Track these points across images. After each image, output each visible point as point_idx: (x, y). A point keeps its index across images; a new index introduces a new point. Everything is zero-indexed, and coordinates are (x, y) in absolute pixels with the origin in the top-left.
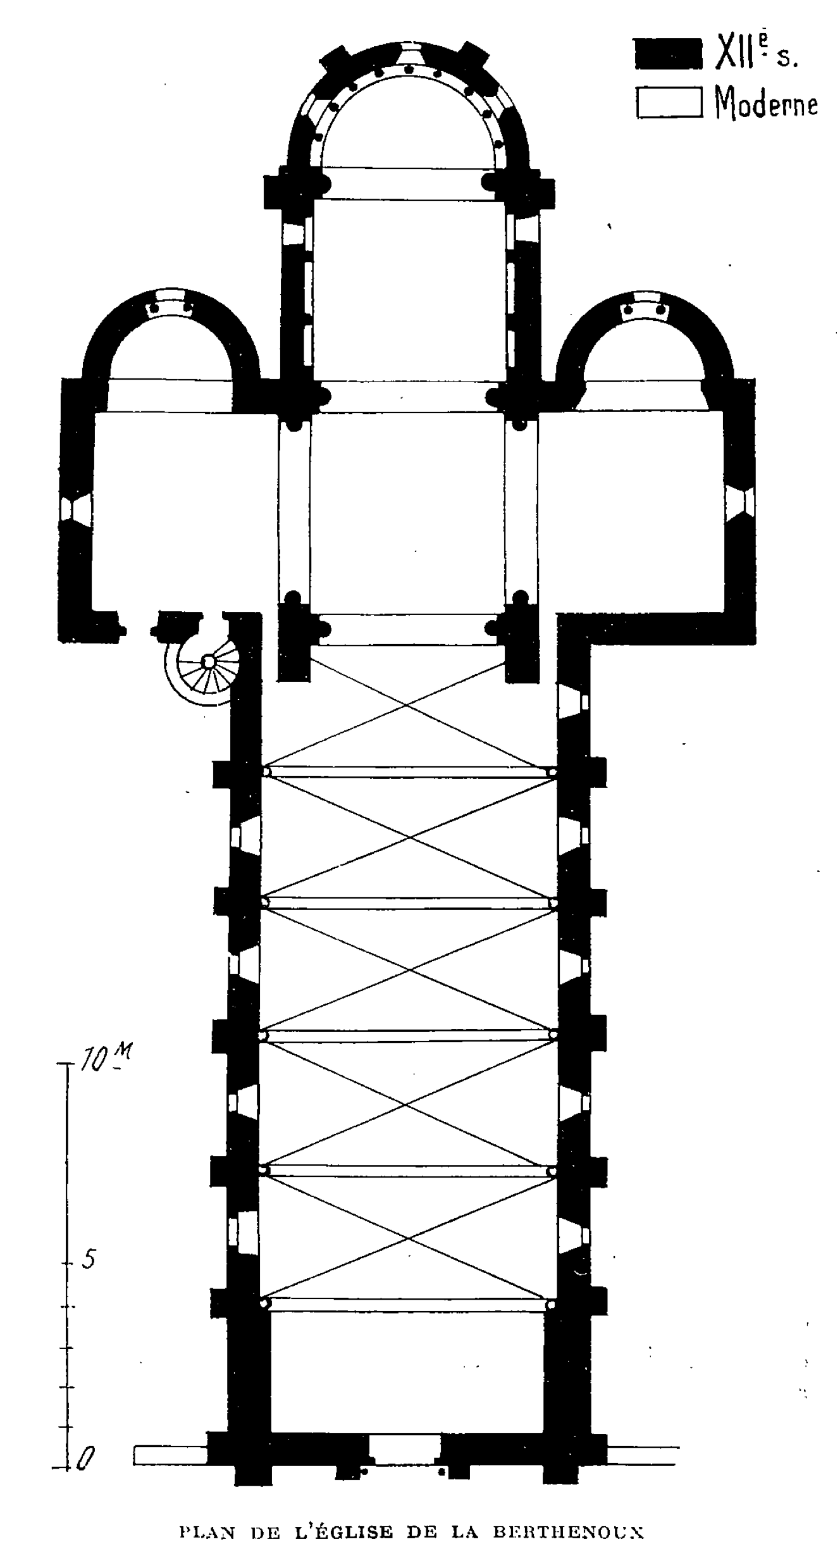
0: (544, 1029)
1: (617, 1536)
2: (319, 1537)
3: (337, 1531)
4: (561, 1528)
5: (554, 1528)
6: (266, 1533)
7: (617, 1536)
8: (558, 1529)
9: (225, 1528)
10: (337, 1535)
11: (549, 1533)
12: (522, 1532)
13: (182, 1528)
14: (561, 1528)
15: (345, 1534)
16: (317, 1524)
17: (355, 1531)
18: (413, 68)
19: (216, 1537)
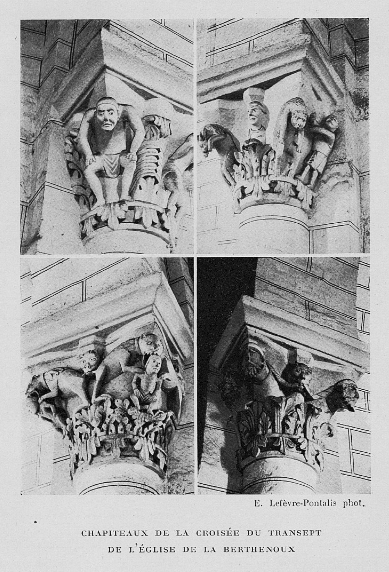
1: (282, 551)
2: (140, 552)
5: (252, 547)
7: (282, 551)
8: (254, 548)
9: (268, 547)
11: (250, 550)
12: (237, 549)
15: (153, 550)
16: (139, 545)
17: (158, 549)
18: (95, 374)
19: (100, 535)
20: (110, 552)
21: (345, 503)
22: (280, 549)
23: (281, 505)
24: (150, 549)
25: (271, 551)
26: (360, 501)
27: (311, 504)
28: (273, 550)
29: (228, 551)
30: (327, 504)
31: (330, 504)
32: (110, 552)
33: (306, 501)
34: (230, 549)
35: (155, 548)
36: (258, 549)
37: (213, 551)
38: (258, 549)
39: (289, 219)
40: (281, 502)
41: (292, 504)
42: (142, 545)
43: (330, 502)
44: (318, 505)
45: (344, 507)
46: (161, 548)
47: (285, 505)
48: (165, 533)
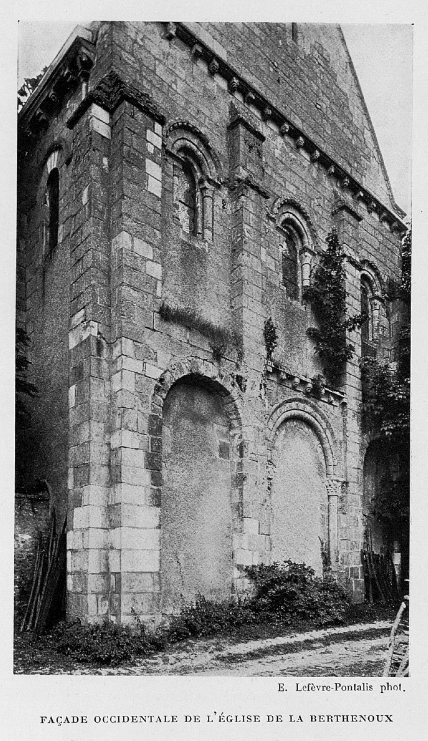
0: (211, 149)
1: (378, 720)
3: (229, 718)
4: (347, 716)
6: (131, 719)
7: (378, 720)
9: (142, 717)
10: (229, 720)
11: (340, 719)
12: (326, 719)
13: (312, 716)
14: (347, 716)
16: (219, 714)
17: (240, 718)
20: (186, 721)
21: (384, 688)
22: (376, 718)
23: (308, 690)
24: (231, 718)
25: (365, 720)
26: (400, 685)
27: (344, 688)
28: (367, 719)
29: (316, 720)
30: (362, 689)
31: (366, 689)
32: (186, 721)
33: (338, 685)
34: (318, 718)
35: (236, 717)
36: (350, 718)
37: (300, 721)
38: (350, 718)
39: (350, 340)
40: (308, 686)
41: (322, 688)
42: (222, 713)
43: (365, 685)
44: (351, 690)
45: (382, 692)
46: (243, 717)
47: (313, 689)
48: (195, 719)
